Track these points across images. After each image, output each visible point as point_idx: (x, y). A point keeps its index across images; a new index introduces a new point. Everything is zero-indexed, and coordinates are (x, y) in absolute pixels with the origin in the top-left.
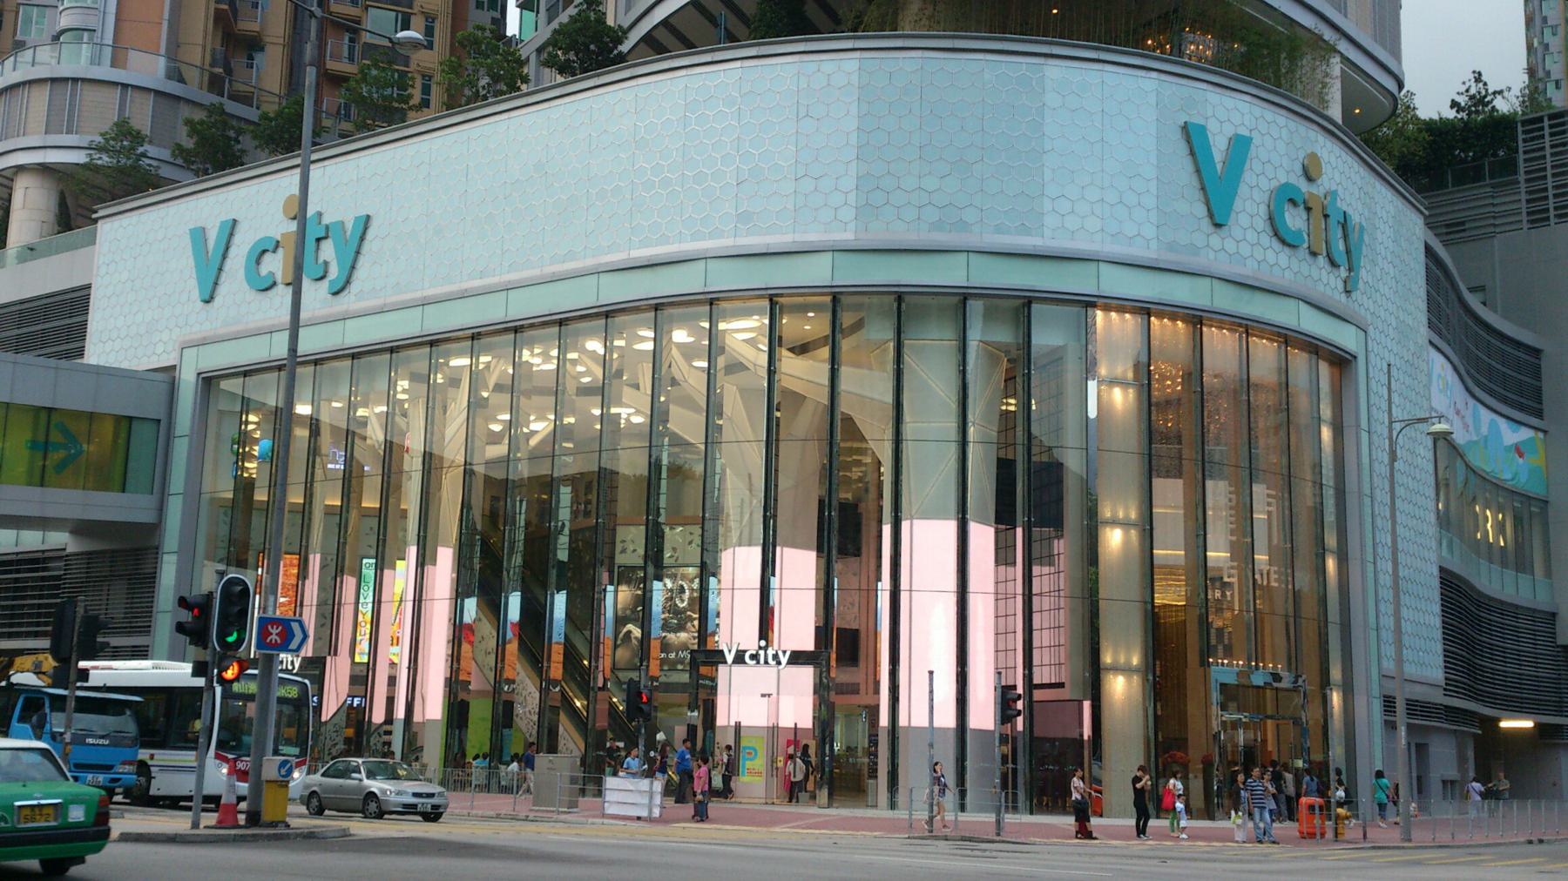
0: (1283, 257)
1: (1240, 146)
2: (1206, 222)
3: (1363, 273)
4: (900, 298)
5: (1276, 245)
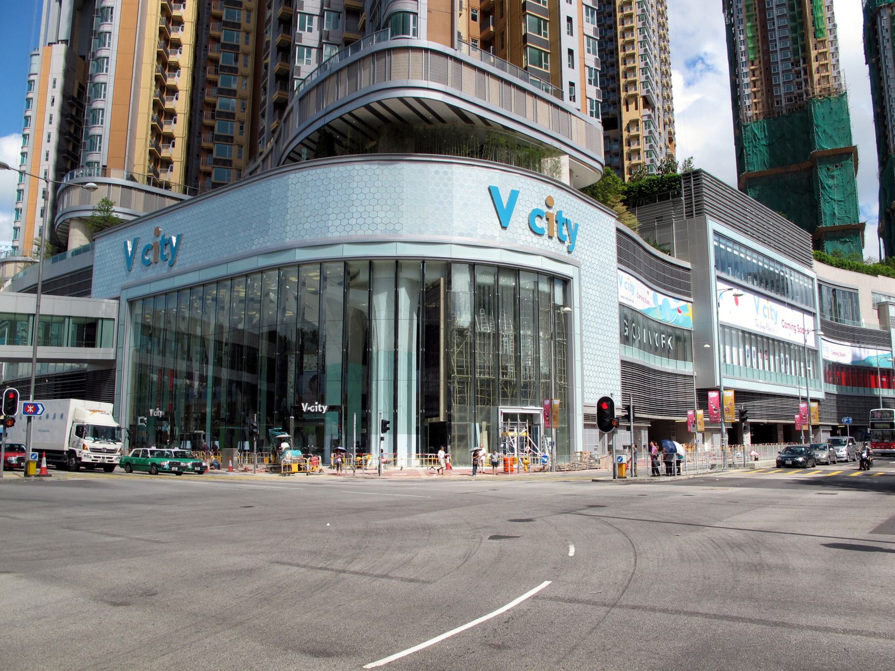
0: (536, 238)
1: (514, 195)
5: (533, 235)
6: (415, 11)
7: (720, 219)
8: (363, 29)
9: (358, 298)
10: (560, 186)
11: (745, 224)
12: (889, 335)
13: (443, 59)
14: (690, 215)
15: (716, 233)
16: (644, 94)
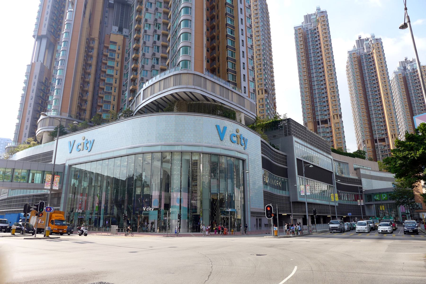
1: (225, 128)
2: (220, 140)
3: (247, 146)
4: (171, 153)
5: (231, 143)
6: (189, 59)
7: (297, 137)
8: (168, 65)
9: (167, 166)
10: (242, 125)
11: (306, 138)
12: (361, 181)
13: (200, 77)
14: (286, 135)
15: (296, 141)
16: (265, 88)
